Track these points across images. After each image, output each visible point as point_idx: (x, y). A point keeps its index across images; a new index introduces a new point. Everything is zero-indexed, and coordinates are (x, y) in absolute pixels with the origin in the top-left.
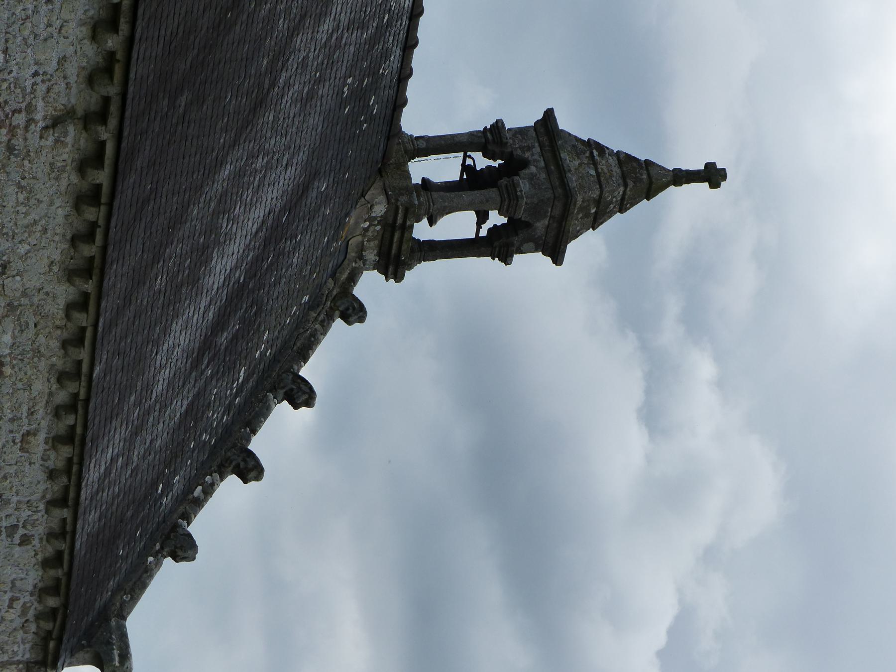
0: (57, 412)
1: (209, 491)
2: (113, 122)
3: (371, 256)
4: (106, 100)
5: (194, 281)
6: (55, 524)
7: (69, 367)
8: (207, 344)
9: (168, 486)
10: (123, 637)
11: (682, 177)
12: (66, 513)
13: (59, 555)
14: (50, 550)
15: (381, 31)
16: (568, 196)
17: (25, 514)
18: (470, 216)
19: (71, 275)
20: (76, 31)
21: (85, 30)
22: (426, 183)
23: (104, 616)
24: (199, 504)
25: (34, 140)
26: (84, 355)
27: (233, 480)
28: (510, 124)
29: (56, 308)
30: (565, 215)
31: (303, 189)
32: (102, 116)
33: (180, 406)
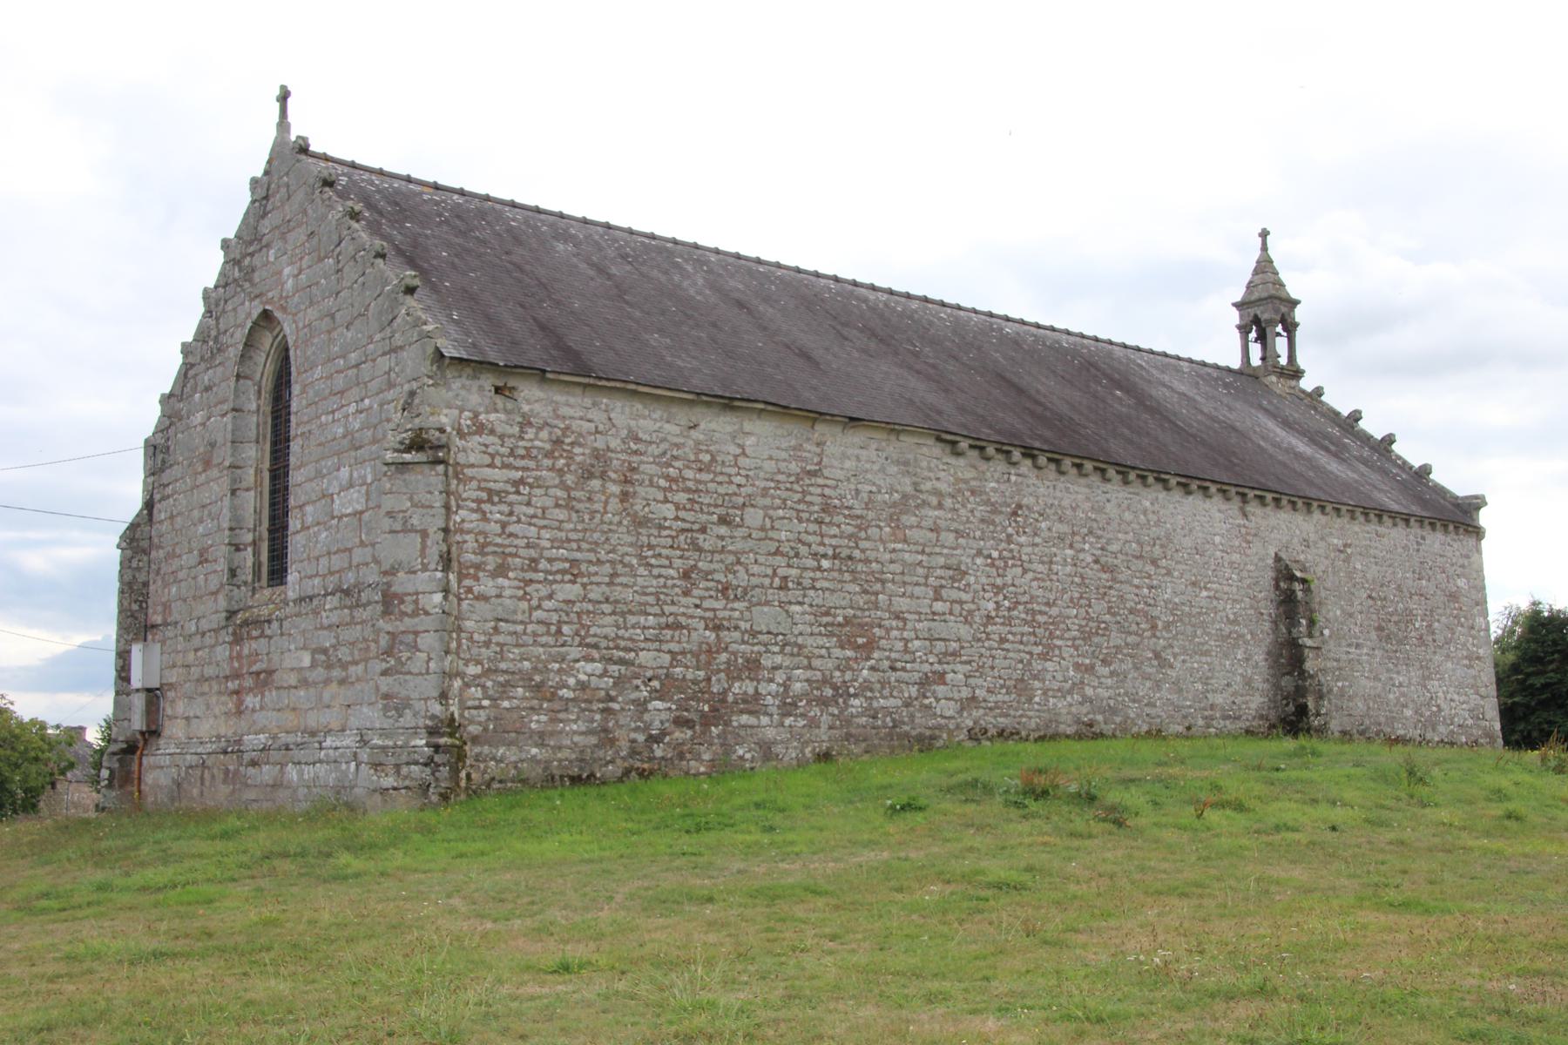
0: (1368, 521)
1: (1399, 458)
2: (1246, 491)
3: (1293, 383)
4: (1237, 493)
5: (1309, 460)
6: (1417, 524)
7: (1349, 515)
8: (1335, 455)
9: (1397, 475)
10: (1467, 497)
11: (1264, 248)
12: (1412, 519)
13: (1431, 524)
14: (1428, 527)
15: (1199, 375)
16: (1271, 297)
17: (1411, 537)
18: (1278, 339)
19: (1309, 512)
20: (1208, 504)
21: (1208, 500)
22: (1263, 359)
23: (1458, 506)
24: (1405, 462)
25: (1252, 525)
26: (1344, 508)
27: (1394, 447)
28: (1237, 322)
29: (1323, 519)
30: (1280, 299)
31: (1266, 411)
32: (1244, 495)
33: (1362, 468)
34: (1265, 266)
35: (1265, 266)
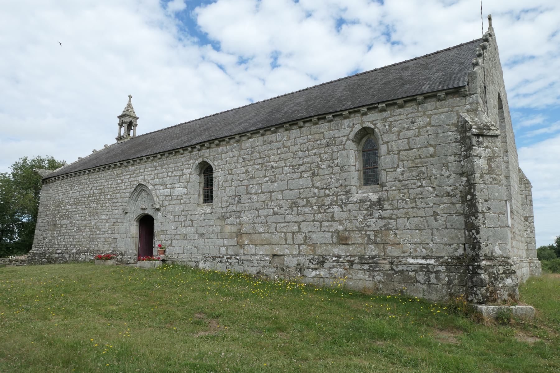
11: (130, 101)
34: (129, 105)
35: (129, 105)
